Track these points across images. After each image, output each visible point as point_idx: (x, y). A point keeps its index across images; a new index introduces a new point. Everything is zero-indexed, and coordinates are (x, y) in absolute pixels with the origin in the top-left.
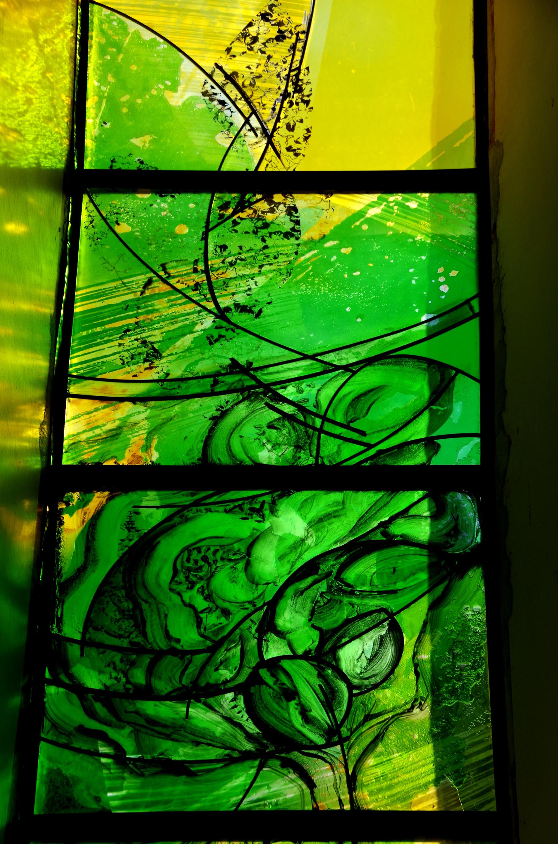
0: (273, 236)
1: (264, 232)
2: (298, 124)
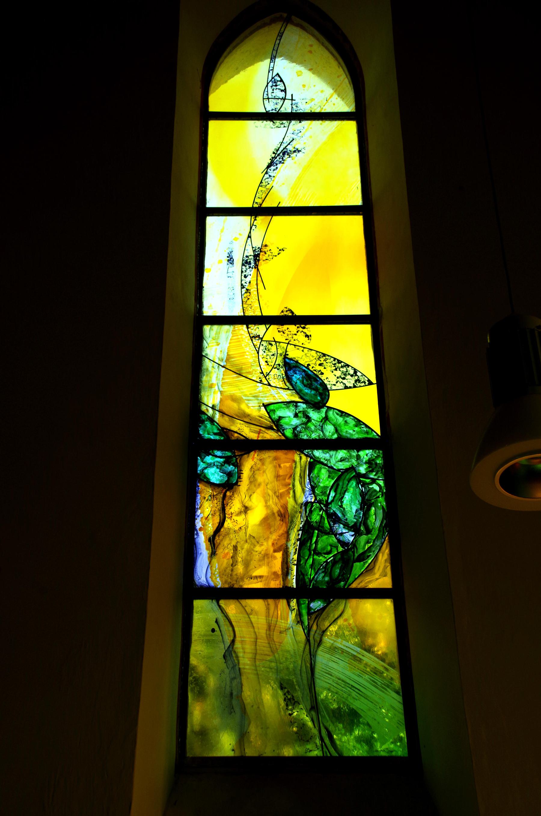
0: (277, 89)
1: (275, 87)
2: (249, 276)
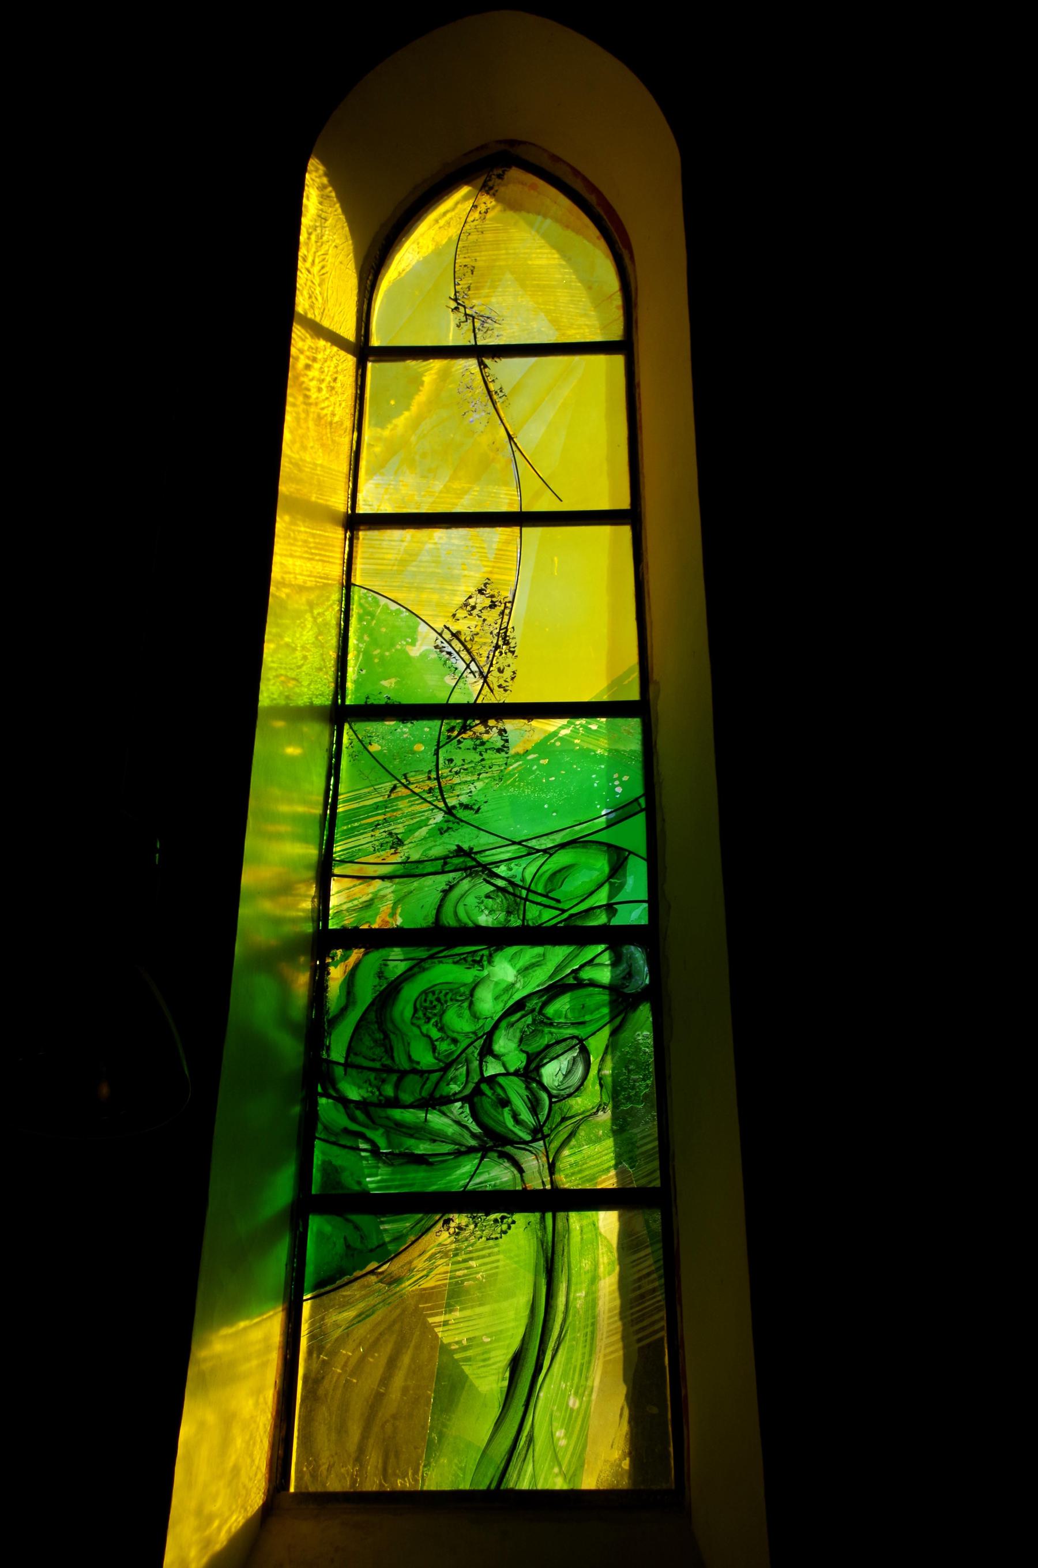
2: (506, 668)
